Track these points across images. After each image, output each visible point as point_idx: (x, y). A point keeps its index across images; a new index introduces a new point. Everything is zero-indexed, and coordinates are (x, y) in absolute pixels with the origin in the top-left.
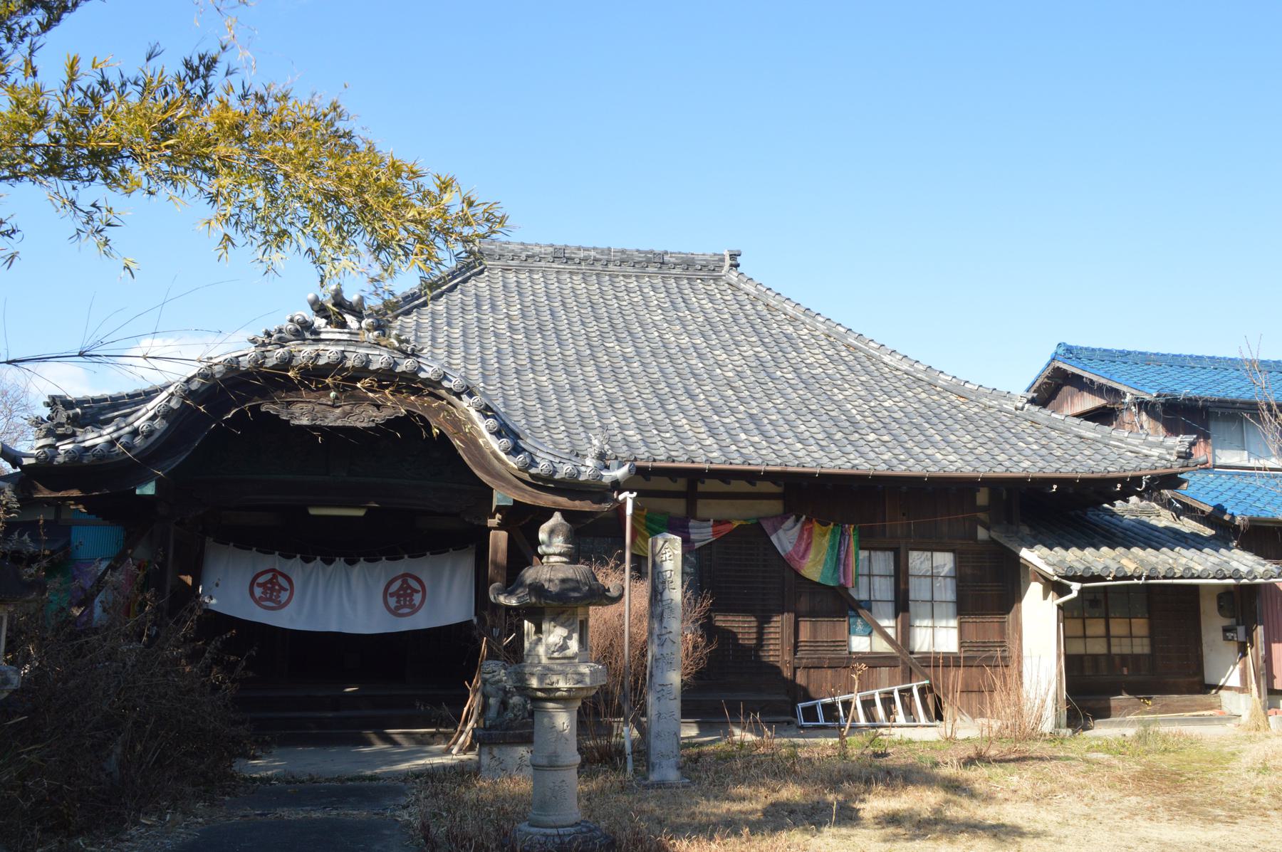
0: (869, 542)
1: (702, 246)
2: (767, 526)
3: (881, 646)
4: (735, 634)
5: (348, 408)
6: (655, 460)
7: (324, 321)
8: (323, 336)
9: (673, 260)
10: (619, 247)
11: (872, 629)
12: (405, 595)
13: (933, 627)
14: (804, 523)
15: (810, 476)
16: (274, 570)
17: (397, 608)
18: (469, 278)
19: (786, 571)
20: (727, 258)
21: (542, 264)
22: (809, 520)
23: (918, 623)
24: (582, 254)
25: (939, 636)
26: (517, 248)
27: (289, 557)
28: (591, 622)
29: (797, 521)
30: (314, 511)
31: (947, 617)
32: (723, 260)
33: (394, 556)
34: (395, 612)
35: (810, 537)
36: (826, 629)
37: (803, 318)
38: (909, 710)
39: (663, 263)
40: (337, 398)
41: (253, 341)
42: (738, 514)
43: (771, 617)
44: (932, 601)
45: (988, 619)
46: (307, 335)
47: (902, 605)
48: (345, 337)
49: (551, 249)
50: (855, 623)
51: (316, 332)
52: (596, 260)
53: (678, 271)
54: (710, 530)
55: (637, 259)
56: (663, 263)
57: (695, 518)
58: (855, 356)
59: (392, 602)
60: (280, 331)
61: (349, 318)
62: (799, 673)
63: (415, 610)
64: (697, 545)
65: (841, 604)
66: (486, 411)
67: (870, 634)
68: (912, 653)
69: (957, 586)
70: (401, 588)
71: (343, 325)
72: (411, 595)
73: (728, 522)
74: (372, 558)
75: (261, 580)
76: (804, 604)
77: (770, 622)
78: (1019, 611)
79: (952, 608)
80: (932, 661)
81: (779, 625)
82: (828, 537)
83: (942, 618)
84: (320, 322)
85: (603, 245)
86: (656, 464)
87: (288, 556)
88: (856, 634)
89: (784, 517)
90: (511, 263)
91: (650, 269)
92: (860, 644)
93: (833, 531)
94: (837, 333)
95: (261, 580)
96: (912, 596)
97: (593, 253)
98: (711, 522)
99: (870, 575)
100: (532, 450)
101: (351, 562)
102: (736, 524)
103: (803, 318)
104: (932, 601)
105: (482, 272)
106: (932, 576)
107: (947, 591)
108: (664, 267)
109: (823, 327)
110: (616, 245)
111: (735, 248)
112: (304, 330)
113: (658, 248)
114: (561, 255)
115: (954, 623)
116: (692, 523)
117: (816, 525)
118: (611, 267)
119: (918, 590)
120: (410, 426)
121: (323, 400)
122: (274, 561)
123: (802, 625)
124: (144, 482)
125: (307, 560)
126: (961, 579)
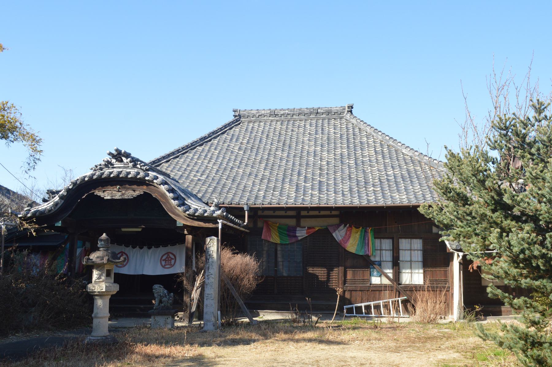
0: (378, 235)
1: (336, 103)
2: (331, 229)
3: (385, 281)
4: (317, 276)
5: (123, 192)
6: (263, 204)
7: (115, 160)
8: (115, 166)
9: (322, 111)
10: (299, 107)
11: (382, 274)
12: (168, 260)
13: (411, 273)
14: (348, 228)
15: (355, 208)
16: (122, 252)
17: (165, 265)
18: (233, 127)
19: (339, 248)
20: (347, 108)
21: (265, 118)
22: (350, 226)
23: (404, 271)
24: (282, 112)
25: (414, 276)
26: (254, 112)
27: (127, 246)
28: (184, 267)
29: (345, 226)
30: (123, 230)
31: (418, 268)
32: (345, 109)
33: (165, 245)
34: (164, 267)
35: (351, 233)
36: (360, 274)
37: (373, 133)
38: (397, 311)
39: (317, 113)
40: (119, 188)
41: (92, 169)
42: (318, 224)
43: (333, 268)
44: (411, 261)
45: (438, 269)
46: (110, 166)
47: (396, 264)
48: (122, 166)
49: (269, 111)
50: (373, 271)
51: (112, 165)
52: (288, 114)
53: (324, 116)
54: (305, 231)
55: (306, 112)
56: (317, 113)
57: (300, 227)
58: (390, 150)
59: (163, 263)
60: (100, 165)
61: (124, 158)
62: (346, 293)
63: (172, 266)
64: (300, 238)
65: (366, 263)
66: (171, 190)
67: (380, 276)
68: (400, 284)
69: (423, 254)
70: (167, 258)
71: (122, 161)
72: (171, 260)
73: (313, 228)
74: (157, 246)
75: (164, 258)
76: (349, 263)
77: (333, 271)
78: (452, 265)
79: (421, 264)
80: (413, 289)
81: (337, 273)
82: (359, 233)
83: (415, 268)
84: (114, 161)
85: (291, 107)
86: (263, 206)
87: (127, 246)
88: (373, 276)
89: (338, 226)
90: (252, 119)
91: (311, 116)
92: (376, 280)
93: (361, 231)
94: (386, 140)
95: (164, 258)
96: (401, 259)
97: (287, 111)
98: (306, 228)
99: (381, 250)
100: (190, 204)
101: (149, 248)
102: (317, 229)
103: (373, 133)
104: (411, 261)
105: (239, 124)
106: (411, 250)
107: (418, 256)
108: (318, 115)
109: (380, 137)
110: (297, 107)
111: (350, 103)
112: (108, 164)
113: (316, 107)
114: (273, 114)
115: (421, 271)
116: (298, 229)
117: (354, 228)
118: (294, 117)
119: (404, 256)
120: (146, 195)
121: (115, 189)
122: (169, 249)
123: (348, 272)
124: (58, 221)
125: (134, 247)
126: (425, 252)
